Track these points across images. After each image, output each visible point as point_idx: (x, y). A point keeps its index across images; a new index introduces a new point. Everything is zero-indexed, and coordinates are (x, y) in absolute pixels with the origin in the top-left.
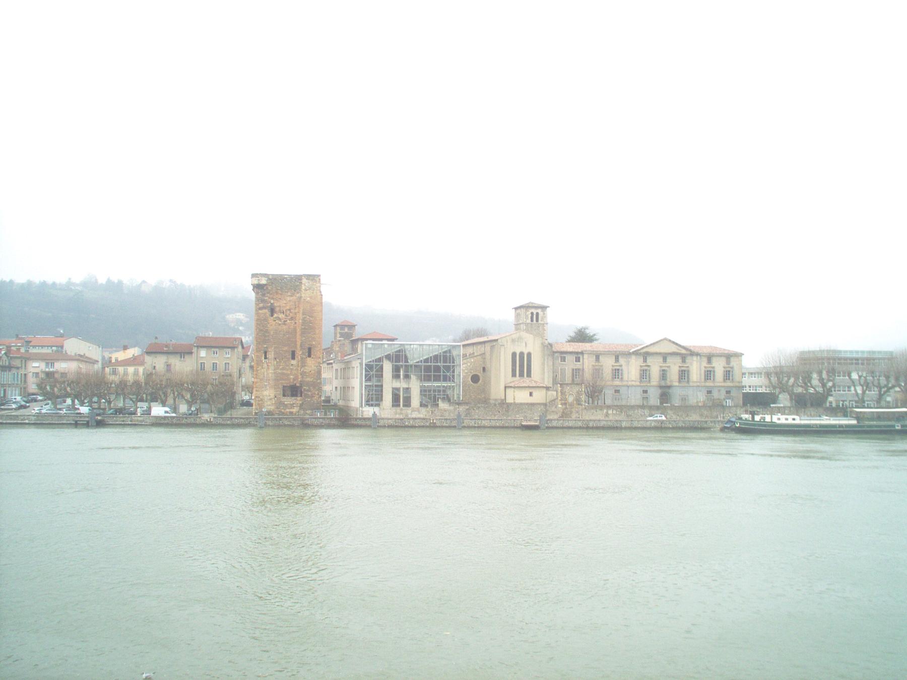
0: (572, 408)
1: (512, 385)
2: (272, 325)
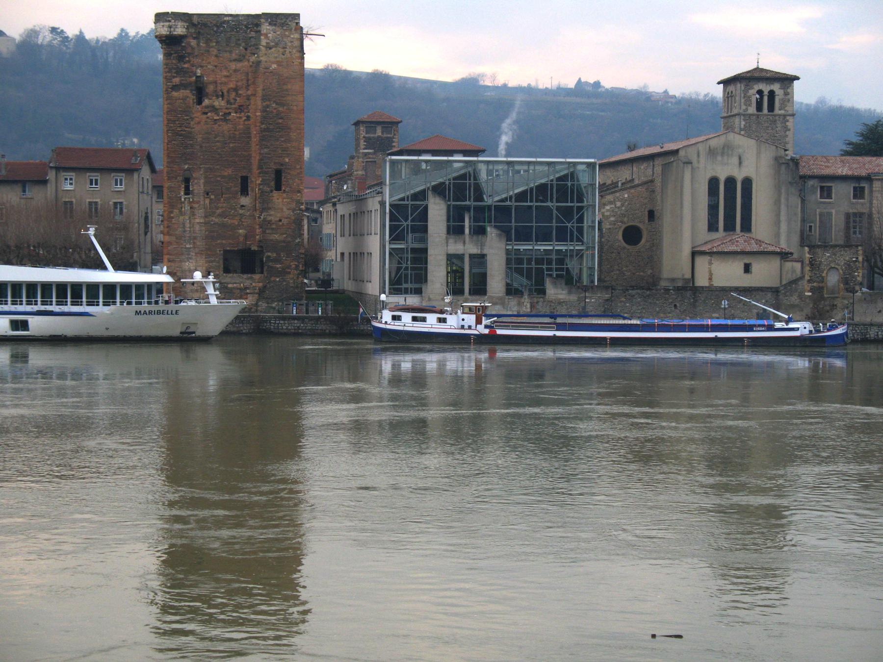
0: (834, 298)
1: (705, 248)
2: (199, 123)
